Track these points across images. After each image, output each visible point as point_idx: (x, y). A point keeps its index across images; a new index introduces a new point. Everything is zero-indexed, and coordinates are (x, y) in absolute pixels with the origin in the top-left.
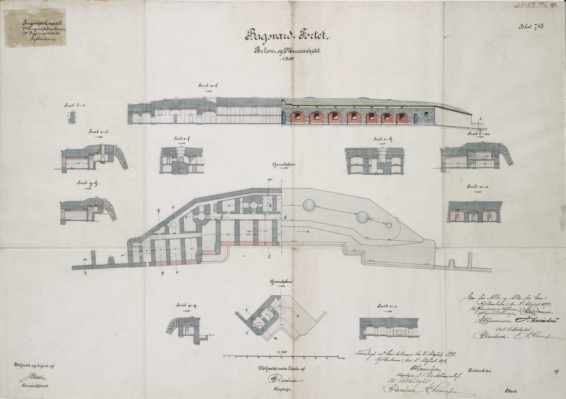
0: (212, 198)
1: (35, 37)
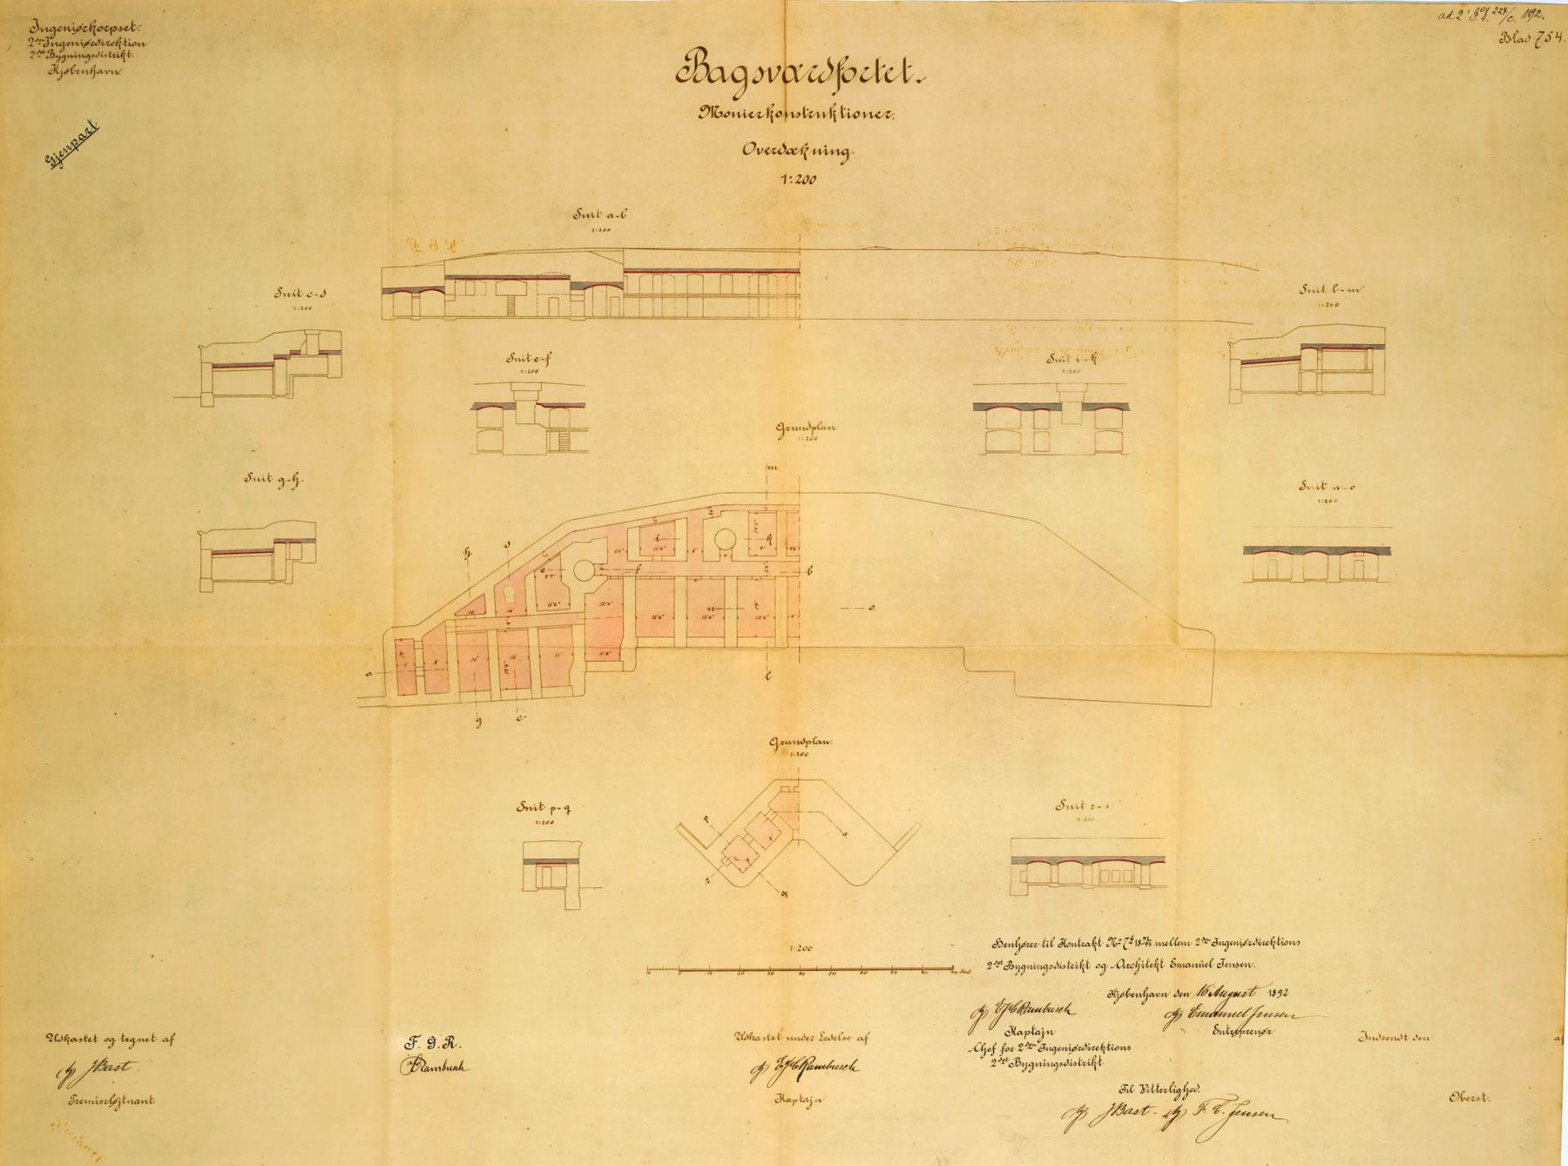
1: (62, 67)
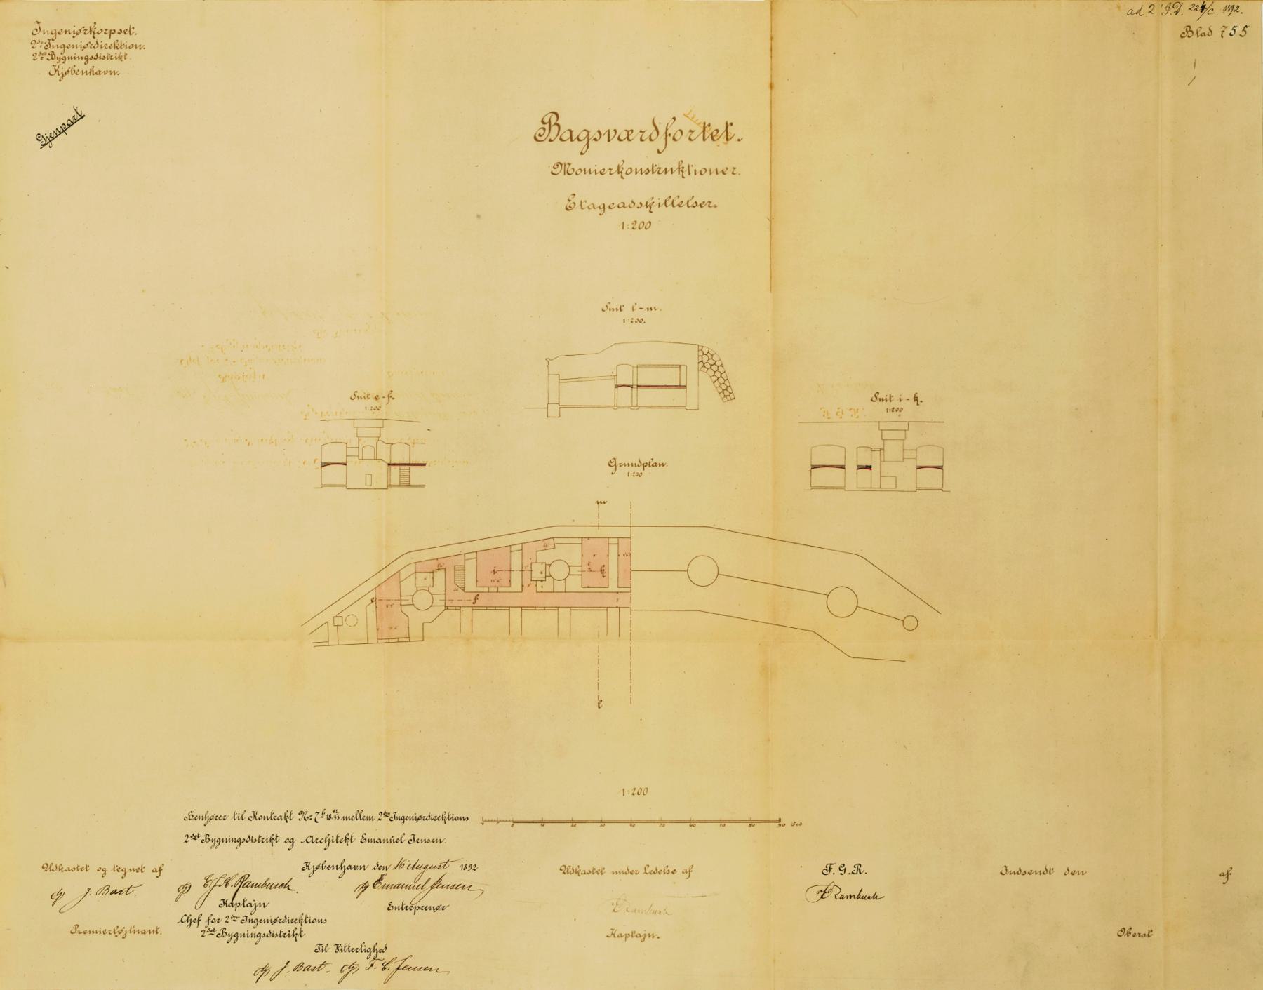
1: (64, 67)
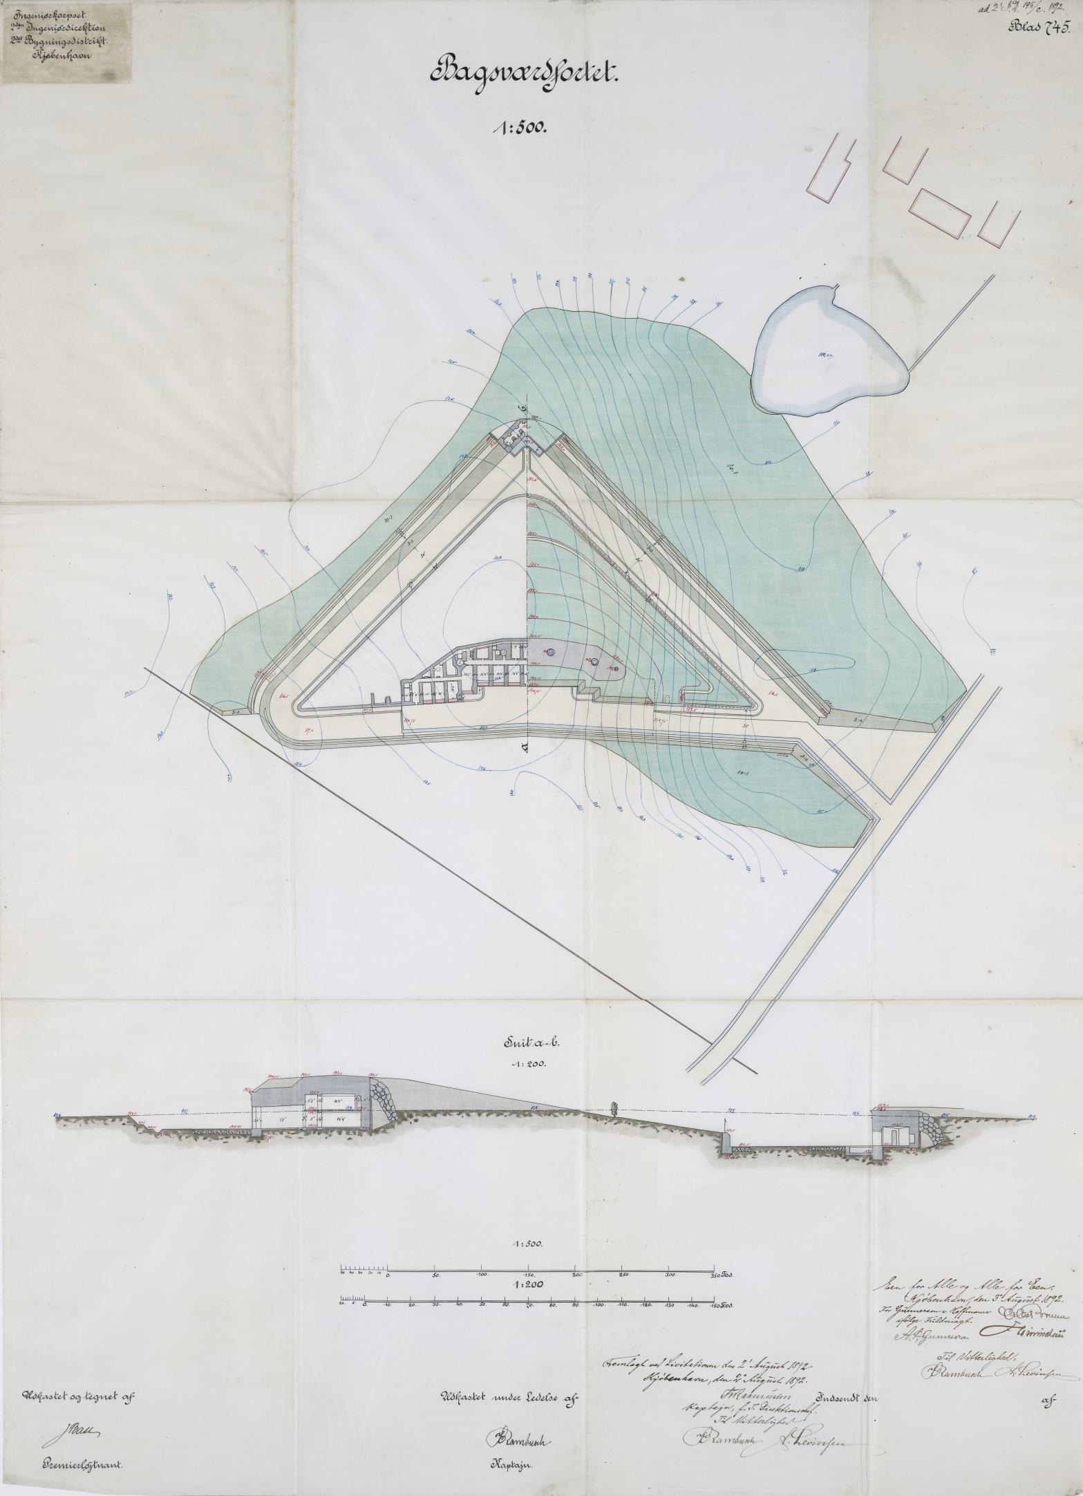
0: (467, 647)
